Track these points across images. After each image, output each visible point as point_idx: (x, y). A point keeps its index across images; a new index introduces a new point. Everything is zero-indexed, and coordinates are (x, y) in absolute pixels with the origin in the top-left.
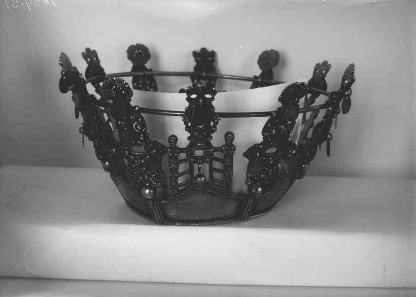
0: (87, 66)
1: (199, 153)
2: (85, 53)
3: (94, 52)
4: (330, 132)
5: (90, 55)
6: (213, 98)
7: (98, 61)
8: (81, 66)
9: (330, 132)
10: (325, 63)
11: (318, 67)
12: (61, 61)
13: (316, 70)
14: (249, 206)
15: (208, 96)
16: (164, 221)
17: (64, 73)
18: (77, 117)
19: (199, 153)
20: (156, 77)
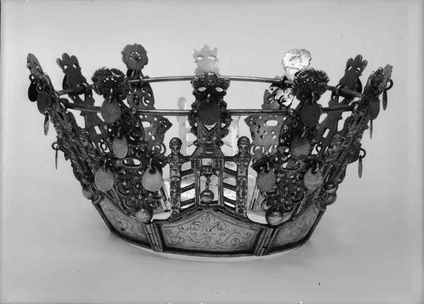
0: (64, 75)
1: (206, 162)
2: (62, 59)
3: (74, 58)
4: (362, 147)
5: (69, 64)
6: (224, 93)
7: (79, 69)
8: (56, 78)
9: (362, 147)
10: (359, 58)
11: (350, 63)
12: (28, 62)
13: (348, 67)
14: (267, 237)
15: (220, 90)
16: (173, 179)
17: (33, 78)
18: (46, 132)
19: (206, 162)
20: (151, 84)
